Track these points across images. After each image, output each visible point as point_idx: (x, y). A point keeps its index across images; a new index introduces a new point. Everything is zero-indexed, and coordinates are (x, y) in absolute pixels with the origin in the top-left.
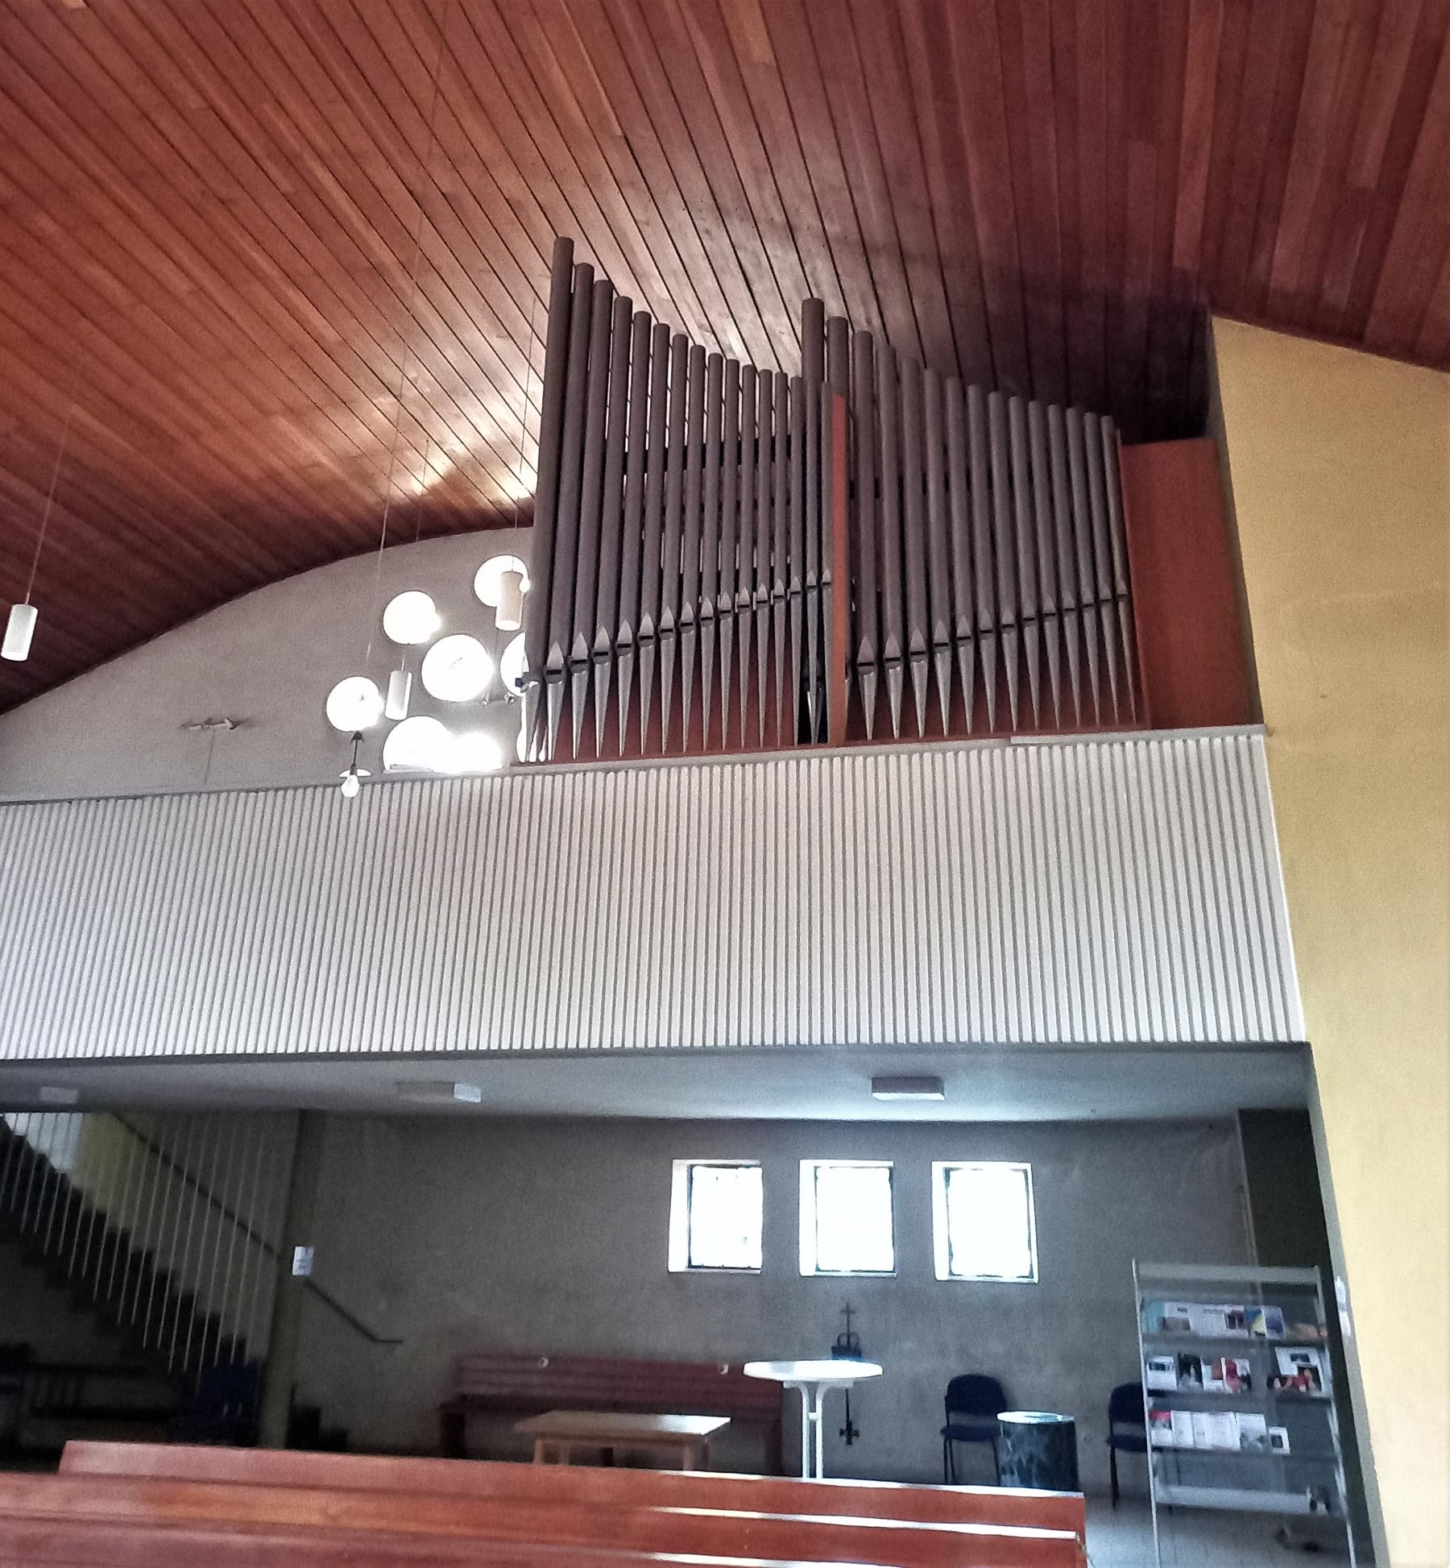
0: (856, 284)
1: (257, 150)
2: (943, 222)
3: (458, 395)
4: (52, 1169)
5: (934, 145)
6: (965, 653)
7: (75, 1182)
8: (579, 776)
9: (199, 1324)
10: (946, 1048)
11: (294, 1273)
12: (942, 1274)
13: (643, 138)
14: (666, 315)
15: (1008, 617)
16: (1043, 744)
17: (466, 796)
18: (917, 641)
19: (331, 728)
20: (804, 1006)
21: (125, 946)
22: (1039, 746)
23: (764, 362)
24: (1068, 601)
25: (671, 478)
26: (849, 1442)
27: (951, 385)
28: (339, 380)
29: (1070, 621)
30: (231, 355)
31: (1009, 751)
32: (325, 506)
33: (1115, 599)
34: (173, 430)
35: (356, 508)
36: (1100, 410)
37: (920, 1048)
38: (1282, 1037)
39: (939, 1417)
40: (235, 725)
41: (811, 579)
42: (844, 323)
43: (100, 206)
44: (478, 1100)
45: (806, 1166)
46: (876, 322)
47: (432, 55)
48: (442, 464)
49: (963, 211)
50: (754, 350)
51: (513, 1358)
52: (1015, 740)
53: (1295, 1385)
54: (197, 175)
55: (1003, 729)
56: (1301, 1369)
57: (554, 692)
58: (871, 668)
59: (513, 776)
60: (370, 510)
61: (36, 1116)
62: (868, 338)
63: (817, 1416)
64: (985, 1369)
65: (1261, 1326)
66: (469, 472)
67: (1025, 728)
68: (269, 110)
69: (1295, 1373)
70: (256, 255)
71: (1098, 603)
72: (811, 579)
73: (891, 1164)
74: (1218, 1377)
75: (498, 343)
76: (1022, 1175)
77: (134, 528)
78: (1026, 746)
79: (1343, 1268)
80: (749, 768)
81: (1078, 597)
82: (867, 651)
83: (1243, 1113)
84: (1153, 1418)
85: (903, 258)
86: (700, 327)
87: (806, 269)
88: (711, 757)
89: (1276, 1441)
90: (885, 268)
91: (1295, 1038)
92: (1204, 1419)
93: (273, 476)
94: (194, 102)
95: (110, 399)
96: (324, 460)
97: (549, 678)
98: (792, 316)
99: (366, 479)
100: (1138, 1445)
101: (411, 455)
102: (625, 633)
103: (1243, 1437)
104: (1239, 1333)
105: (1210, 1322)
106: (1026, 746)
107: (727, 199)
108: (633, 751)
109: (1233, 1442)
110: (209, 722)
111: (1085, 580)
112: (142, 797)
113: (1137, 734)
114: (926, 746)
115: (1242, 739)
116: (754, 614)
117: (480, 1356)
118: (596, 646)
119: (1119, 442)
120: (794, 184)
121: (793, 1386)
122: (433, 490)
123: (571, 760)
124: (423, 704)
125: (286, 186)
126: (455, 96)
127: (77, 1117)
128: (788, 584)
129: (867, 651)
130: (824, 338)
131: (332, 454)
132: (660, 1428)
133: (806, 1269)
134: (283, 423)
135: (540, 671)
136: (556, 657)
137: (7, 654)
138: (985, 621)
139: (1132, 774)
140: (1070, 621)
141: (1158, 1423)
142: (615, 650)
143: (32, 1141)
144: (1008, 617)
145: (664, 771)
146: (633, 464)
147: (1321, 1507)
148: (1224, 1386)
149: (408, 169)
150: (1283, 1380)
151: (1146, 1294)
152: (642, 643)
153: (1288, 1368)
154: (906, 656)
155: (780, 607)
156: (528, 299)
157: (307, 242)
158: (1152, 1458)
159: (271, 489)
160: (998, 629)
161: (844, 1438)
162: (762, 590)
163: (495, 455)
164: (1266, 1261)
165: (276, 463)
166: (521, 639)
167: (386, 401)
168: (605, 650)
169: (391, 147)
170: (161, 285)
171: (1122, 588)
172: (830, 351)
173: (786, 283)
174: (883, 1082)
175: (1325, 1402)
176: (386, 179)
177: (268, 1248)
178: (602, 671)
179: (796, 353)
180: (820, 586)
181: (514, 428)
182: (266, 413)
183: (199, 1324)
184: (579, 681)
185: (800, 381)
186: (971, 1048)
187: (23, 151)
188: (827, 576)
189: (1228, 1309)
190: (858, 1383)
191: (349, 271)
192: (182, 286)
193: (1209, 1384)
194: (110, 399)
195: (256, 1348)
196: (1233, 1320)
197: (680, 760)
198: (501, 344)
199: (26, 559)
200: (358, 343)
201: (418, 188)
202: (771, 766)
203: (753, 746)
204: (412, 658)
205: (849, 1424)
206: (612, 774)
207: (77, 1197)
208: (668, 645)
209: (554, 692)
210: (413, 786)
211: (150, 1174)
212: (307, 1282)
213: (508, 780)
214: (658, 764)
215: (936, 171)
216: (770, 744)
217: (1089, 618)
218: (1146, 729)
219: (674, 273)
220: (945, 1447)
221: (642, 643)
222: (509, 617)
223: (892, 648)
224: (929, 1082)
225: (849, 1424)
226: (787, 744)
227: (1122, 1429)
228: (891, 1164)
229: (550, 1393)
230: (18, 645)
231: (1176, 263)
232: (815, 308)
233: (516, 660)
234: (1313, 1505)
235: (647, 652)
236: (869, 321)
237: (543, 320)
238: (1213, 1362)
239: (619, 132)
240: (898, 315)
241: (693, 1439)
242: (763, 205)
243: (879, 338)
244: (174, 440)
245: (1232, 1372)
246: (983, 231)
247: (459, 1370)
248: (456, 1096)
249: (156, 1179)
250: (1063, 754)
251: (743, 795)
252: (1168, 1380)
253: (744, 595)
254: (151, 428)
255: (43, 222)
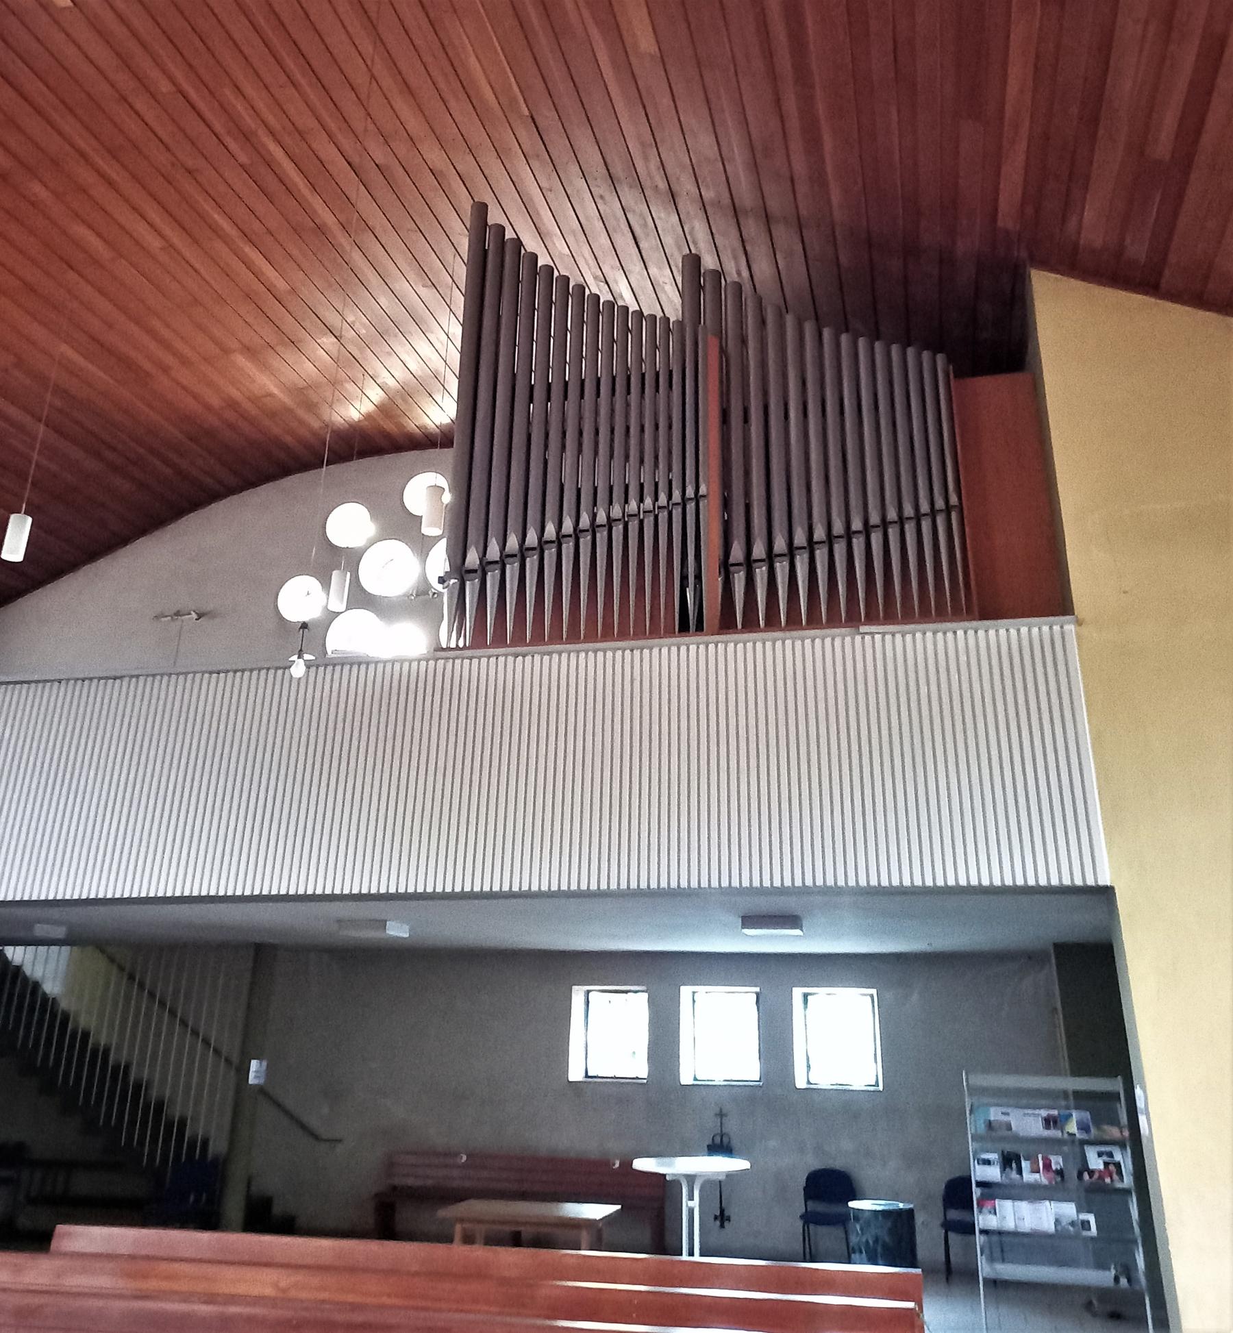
0: (728, 241)
1: (218, 127)
2: (802, 189)
3: (390, 336)
4: (44, 994)
5: (794, 124)
6: (821, 555)
7: (64, 1005)
8: (493, 660)
9: (170, 1126)
10: (804, 891)
11: (250, 1082)
12: (801, 1083)
13: (547, 117)
14: (566, 268)
15: (857, 525)
16: (887, 633)
17: (396, 677)
18: (780, 545)
19: (282, 619)
20: (684, 855)
21: (106, 804)
22: (884, 634)
23: (650, 307)
24: (909, 511)
25: (571, 406)
26: (722, 1226)
27: (809, 328)
28: (288, 323)
29: (910, 528)
30: (196, 301)
31: (858, 638)
32: (276, 430)
33: (948, 509)
34: (147, 366)
35: (302, 432)
36: (936, 349)
37: (783, 891)
38: (1090, 882)
39: (799, 1205)
40: (200, 616)
41: (690, 492)
42: (718, 275)
43: (85, 176)
44: (406, 935)
45: (686, 991)
46: (745, 273)
47: (367, 47)
48: (376, 395)
49: (819, 179)
50: (641, 298)
51: (437, 1154)
52: (863, 629)
53: (1101, 1178)
54: (168, 149)
55: (853, 620)
56: (1106, 1164)
57: (471, 589)
58: (741, 568)
59: (437, 660)
60: (314, 434)
61: (31, 949)
62: (739, 287)
63: (695, 1203)
64: (838, 1164)
65: (1072, 1127)
66: (399, 402)
67: (871, 618)
68: (228, 93)
69: (1102, 1167)
70: (217, 217)
71: (933, 513)
72: (690, 492)
73: (758, 989)
74: (1036, 1170)
75: (423, 291)
76: (869, 999)
77: (114, 449)
78: (872, 634)
79: (1142, 1078)
80: (637, 653)
81: (917, 507)
82: (737, 553)
83: (1057, 946)
84: (980, 1206)
85: (768, 219)
86: (596, 278)
87: (686, 229)
88: (605, 643)
89: (1085, 1225)
90: (752, 228)
91: (1101, 883)
92: (1024, 1206)
93: (232, 404)
94: (165, 87)
95: (93, 339)
96: (276, 391)
97: (467, 576)
98: (673, 268)
99: (311, 407)
100: (968, 1229)
101: (350, 387)
102: (532, 538)
103: (1057, 1222)
104: (1054, 1133)
105: (1029, 1124)
106: (872, 634)
107: (618, 169)
108: (538, 639)
109: (1049, 1226)
110: (178, 614)
111: (923, 493)
112: (121, 678)
113: (966, 624)
114: (788, 634)
115: (1056, 628)
116: (641, 522)
117: (408, 1153)
118: (507, 549)
119: (952, 376)
120: (675, 156)
121: (674, 1178)
122: (368, 417)
123: (485, 646)
124: (360, 598)
125: (243, 158)
126: (387, 81)
127: (66, 950)
128: (670, 497)
129: (737, 553)
130: (700, 288)
131: (283, 386)
132: (561, 1214)
133: (686, 1079)
134: (241, 360)
135: (460, 570)
136: (473, 558)
137: (6, 556)
138: (838, 528)
139: (963, 658)
140: (910, 528)
141: (985, 1210)
142: (523, 552)
143: (27, 970)
144: (857, 525)
145: (564, 656)
146: (539, 394)
147: (1124, 1282)
148: (1041, 1178)
149: (347, 143)
150: (1091, 1173)
151: (975, 1100)
152: (546, 546)
153: (1096, 1163)
154: (771, 557)
155: (663, 516)
156: (449, 254)
157: (261, 206)
158: (979, 1239)
159: (230, 415)
160: (849, 534)
161: (718, 1223)
162: (648, 502)
163: (421, 387)
164: (1077, 1072)
165: (235, 393)
166: (443, 544)
167: (328, 341)
168: (514, 553)
169: (332, 125)
170: (137, 243)
171: (954, 500)
172: (706, 299)
173: (668, 241)
174: (751, 920)
175: (1127, 1192)
176: (328, 152)
177: (228, 1061)
178: (512, 570)
179: (677, 300)
180: (697, 498)
181: (437, 364)
182: (226, 351)
183: (170, 1126)
184: (492, 579)
185: (680, 324)
186: (826, 891)
187: (19, 129)
188: (703, 490)
189: (1044, 1113)
190: (730, 1176)
191: (296, 230)
192: (155, 243)
193: (1028, 1177)
194: (93, 339)
195: (218, 1146)
196: (1049, 1122)
197: (578, 646)
198: (426, 292)
199: (22, 476)
200: (305, 292)
201: (356, 160)
202: (655, 651)
203: (640, 634)
204: (350, 559)
205: (722, 1211)
206: (520, 658)
207: (66, 1017)
208: (568, 548)
209: (471, 589)
210: (351, 668)
211: (128, 998)
212: (261, 1090)
213: (432, 663)
214: (559, 649)
215: (796, 145)
216: (655, 633)
217: (926, 525)
218: (974, 620)
219: (574, 232)
220: (804, 1230)
221: (546, 546)
222: (433, 524)
223: (759, 551)
224: (790, 920)
225: (722, 1211)
226: (669, 633)
227: (954, 1215)
228: (758, 989)
229: (467, 1184)
230: (15, 548)
231: (1000, 224)
232: (693, 262)
233: (439, 561)
234: (1117, 1279)
235: (550, 554)
236: (739, 273)
237: (461, 272)
238: (1032, 1158)
239: (526, 112)
240: (763, 268)
241: (589, 1224)
242: (649, 174)
243: (747, 287)
244: (148, 374)
245: (1048, 1166)
246: (836, 196)
247: (390, 1165)
248: (387, 932)
249: (133, 1002)
250: (904, 641)
251: (632, 676)
252: (993, 1173)
253: (633, 506)
254: (128, 364)
255: (37, 188)
